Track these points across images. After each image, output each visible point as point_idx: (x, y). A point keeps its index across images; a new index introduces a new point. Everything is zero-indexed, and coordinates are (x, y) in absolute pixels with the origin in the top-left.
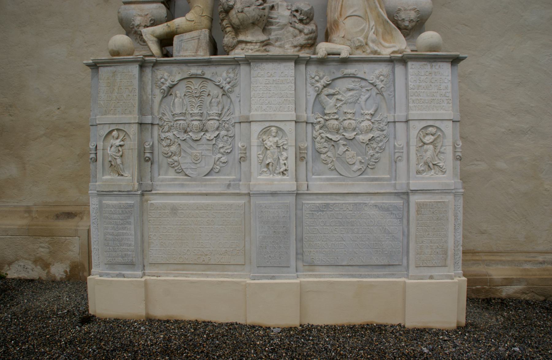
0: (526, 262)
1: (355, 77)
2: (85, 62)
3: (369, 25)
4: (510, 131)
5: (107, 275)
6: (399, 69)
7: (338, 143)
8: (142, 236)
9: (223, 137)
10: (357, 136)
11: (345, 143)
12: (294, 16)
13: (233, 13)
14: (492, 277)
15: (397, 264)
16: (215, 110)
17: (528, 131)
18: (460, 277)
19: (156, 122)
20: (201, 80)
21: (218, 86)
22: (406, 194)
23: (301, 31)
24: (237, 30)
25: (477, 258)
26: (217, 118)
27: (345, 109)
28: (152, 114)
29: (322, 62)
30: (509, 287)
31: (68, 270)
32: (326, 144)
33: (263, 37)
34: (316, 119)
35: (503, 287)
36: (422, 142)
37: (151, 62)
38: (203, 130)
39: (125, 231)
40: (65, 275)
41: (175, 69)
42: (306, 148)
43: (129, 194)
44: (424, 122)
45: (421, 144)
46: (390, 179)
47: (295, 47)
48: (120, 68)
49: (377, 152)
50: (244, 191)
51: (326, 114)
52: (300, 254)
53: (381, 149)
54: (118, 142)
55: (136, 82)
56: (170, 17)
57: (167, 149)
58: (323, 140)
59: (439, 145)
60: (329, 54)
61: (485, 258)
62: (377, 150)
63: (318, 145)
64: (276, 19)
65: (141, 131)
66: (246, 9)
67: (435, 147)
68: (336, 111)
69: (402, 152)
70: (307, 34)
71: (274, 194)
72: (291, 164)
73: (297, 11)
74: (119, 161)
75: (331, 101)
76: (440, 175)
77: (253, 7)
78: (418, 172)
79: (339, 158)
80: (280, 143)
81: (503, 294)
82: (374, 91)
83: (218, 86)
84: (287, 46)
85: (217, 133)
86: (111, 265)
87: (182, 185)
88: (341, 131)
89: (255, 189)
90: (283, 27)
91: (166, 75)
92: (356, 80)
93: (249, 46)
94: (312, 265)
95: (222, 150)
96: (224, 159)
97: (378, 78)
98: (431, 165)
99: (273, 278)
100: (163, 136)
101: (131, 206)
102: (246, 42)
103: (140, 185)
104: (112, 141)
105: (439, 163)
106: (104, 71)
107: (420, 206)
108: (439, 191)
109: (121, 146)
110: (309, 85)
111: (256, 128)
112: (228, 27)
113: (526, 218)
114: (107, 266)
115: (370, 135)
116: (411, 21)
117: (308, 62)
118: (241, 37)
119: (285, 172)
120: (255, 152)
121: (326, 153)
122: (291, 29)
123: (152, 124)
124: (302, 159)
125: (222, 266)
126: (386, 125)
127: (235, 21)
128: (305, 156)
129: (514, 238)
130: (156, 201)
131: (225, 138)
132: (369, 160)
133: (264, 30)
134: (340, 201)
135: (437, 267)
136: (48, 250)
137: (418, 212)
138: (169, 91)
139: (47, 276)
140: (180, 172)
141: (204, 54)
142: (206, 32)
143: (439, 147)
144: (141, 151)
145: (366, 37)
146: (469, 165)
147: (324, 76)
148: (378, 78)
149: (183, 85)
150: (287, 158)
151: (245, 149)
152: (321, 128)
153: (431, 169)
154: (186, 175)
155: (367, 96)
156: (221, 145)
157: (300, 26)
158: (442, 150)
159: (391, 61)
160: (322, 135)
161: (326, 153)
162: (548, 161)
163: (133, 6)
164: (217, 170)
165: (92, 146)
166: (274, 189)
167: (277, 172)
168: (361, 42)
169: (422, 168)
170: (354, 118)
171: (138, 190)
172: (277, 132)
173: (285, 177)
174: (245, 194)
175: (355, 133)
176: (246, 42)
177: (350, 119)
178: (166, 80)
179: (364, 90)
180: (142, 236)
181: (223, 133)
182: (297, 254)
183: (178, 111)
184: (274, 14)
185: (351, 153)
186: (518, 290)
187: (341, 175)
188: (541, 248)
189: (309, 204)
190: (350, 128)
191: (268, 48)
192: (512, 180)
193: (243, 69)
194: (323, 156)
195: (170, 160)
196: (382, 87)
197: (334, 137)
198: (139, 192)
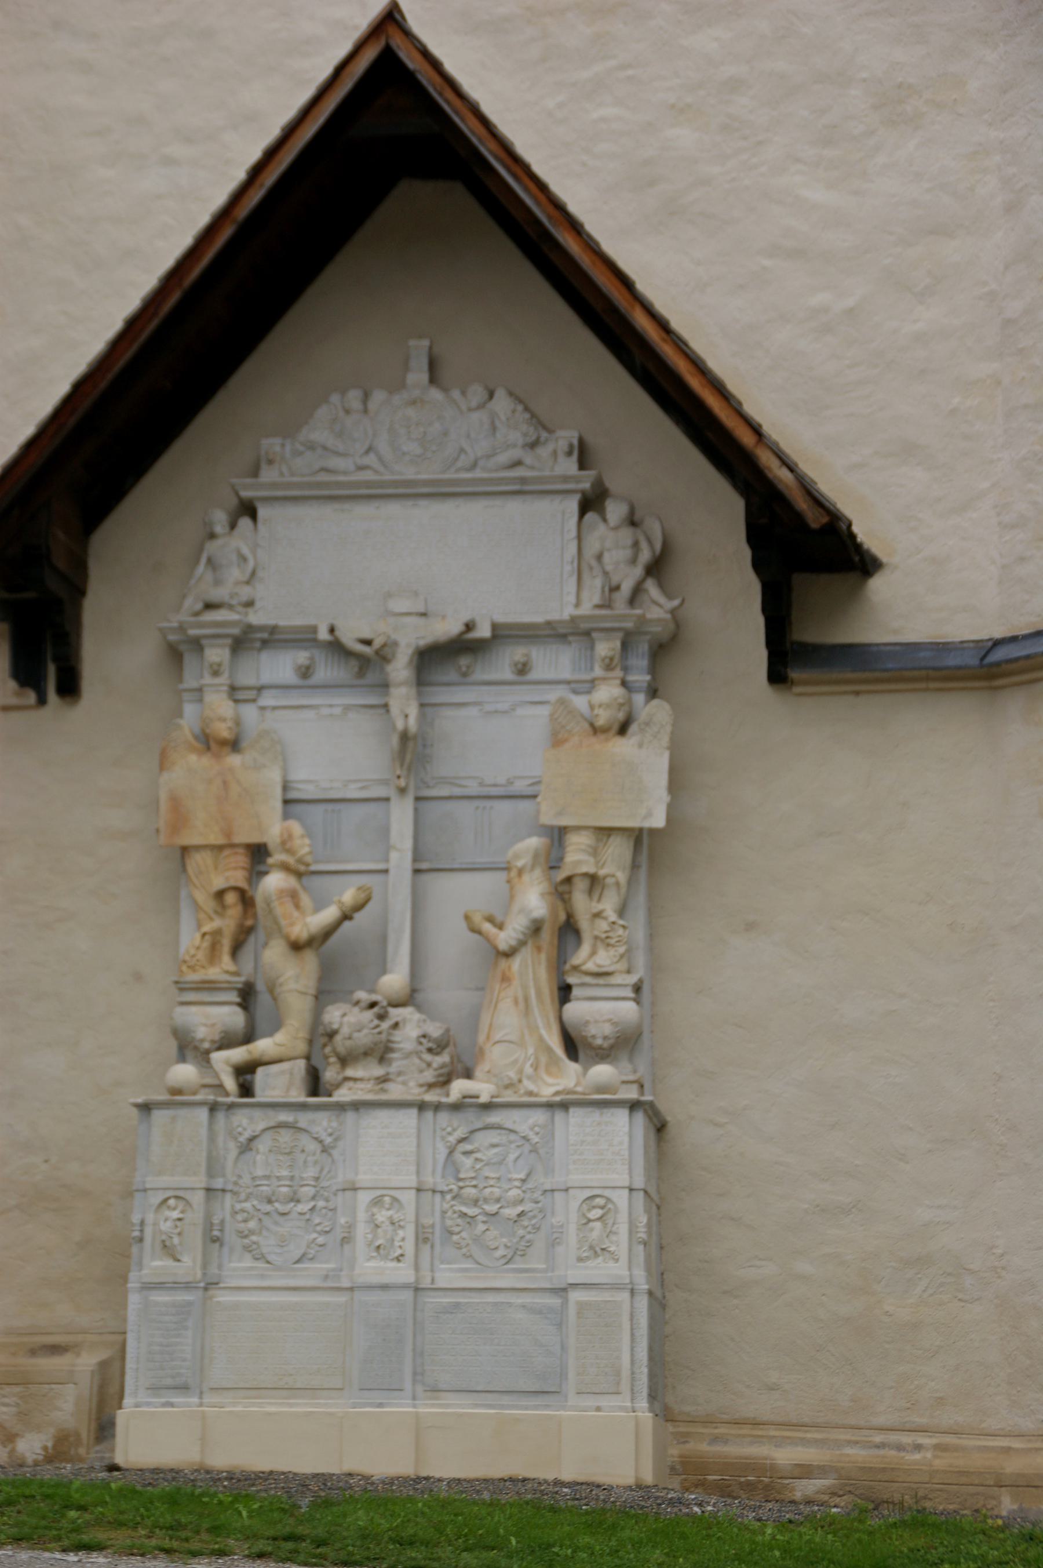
0: (849, 1443)
1: (499, 1127)
2: (132, 1100)
3: (526, 1053)
4: (818, 1208)
5: (148, 1404)
6: (559, 1116)
7: (475, 1219)
8: (202, 1348)
9: (320, 1210)
10: (502, 1210)
11: (485, 1219)
12: (421, 1043)
13: (338, 1038)
14: (774, 1462)
15: (553, 1390)
16: (311, 1172)
17: (853, 1208)
18: (643, 1412)
19: (230, 1187)
20: (292, 1131)
21: (316, 1139)
22: (561, 1291)
23: (429, 1065)
24: (344, 1061)
25: (760, 1433)
26: (312, 1183)
27: (487, 1172)
28: (224, 1176)
29: (456, 1107)
30: (807, 1480)
31: (50, 1444)
32: (459, 1221)
33: (379, 1071)
34: (448, 1185)
35: (794, 1480)
36: (586, 1218)
37: (223, 1104)
38: (295, 1199)
39: (178, 1340)
40: (43, 1453)
41: (257, 1113)
42: (433, 1226)
43: (188, 1286)
44: (589, 1190)
45: (584, 1221)
46: (545, 1271)
47: (421, 1086)
48: (183, 1112)
49: (529, 1233)
50: (346, 1283)
51: (461, 1180)
52: (418, 1375)
53: (534, 1229)
54: (175, 1214)
55: (204, 1132)
56: (248, 1037)
57: (242, 1225)
58: (456, 1215)
59: (610, 1222)
60: (464, 1097)
61: (772, 1433)
62: (529, 1229)
63: (449, 1223)
64: (398, 1042)
65: (208, 1200)
66: (356, 1035)
67: (605, 1225)
68: (473, 1175)
69: (562, 1232)
70: (436, 1070)
71: (385, 1287)
72: (409, 1247)
73: (424, 1036)
74: (176, 1240)
75: (468, 1162)
76: (611, 1264)
77: (365, 1031)
78: (580, 1259)
79: (477, 1240)
80: (396, 1217)
81: (795, 1493)
82: (527, 1148)
83: (316, 1139)
84: (412, 1084)
85: (312, 1204)
86: (155, 1389)
87: (262, 1277)
88: (480, 1203)
89: (361, 1280)
90: (408, 1055)
91: (245, 1122)
92: (503, 1132)
93: (360, 1085)
94: (435, 1390)
95: (319, 1228)
96: (321, 1240)
97: (531, 1129)
98: (598, 1249)
99: (381, 1405)
100: (238, 1206)
101: (190, 1304)
102: (355, 1080)
103: (204, 1274)
104: (167, 1213)
105: (609, 1247)
106: (159, 1116)
107: (582, 1306)
108: (608, 1286)
109: (180, 1219)
110: (438, 1139)
111: (364, 1198)
112: (332, 1056)
113: (851, 1364)
114: (149, 1391)
115: (520, 1209)
116: (605, 1038)
117: (437, 1107)
118: (350, 1072)
119: (401, 1258)
120: (362, 1230)
121: (459, 1233)
122: (417, 1061)
123: (224, 1191)
124: (426, 1240)
125: (312, 1391)
126: (542, 1195)
127: (341, 1050)
128: (430, 1236)
129: (831, 1400)
130: (223, 1298)
131: (324, 1211)
132: (518, 1243)
133: (382, 1060)
134: (476, 1299)
135: (606, 1395)
136: (14, 1409)
137: (579, 1314)
138: (248, 1144)
139: (10, 1457)
140: (261, 1257)
141: (298, 1095)
142: (301, 1064)
143: (610, 1225)
144: (209, 1226)
145: (521, 1071)
146: (744, 1268)
147: (459, 1127)
148: (531, 1129)
149: (267, 1138)
150: (403, 1239)
151: (350, 1227)
152: (454, 1198)
153: (599, 1256)
154: (268, 1262)
155: (516, 1155)
156: (317, 1221)
157: (428, 1057)
158: (614, 1229)
159: (550, 1106)
160: (455, 1208)
161: (459, 1233)
162: (890, 1262)
163: (194, 1009)
164: (311, 1256)
165: (136, 1219)
166: (385, 1280)
167: (390, 1258)
168: (510, 1078)
169: (585, 1254)
170: (498, 1185)
171: (199, 1282)
172: (391, 1204)
173: (400, 1265)
174: (347, 1289)
175: (498, 1206)
176: (355, 1080)
177: (492, 1186)
178: (245, 1129)
179: (513, 1146)
180: (202, 1348)
181: (321, 1203)
182: (415, 1374)
183: (259, 1172)
184: (397, 1036)
185: (493, 1233)
186: (823, 1488)
187: (479, 1264)
188: (881, 1420)
189: (432, 1302)
190: (492, 1199)
191: (386, 1086)
192: (824, 1295)
193: (350, 1116)
194: (455, 1238)
195: (246, 1241)
196: (537, 1143)
197: (471, 1211)
198: (202, 1285)
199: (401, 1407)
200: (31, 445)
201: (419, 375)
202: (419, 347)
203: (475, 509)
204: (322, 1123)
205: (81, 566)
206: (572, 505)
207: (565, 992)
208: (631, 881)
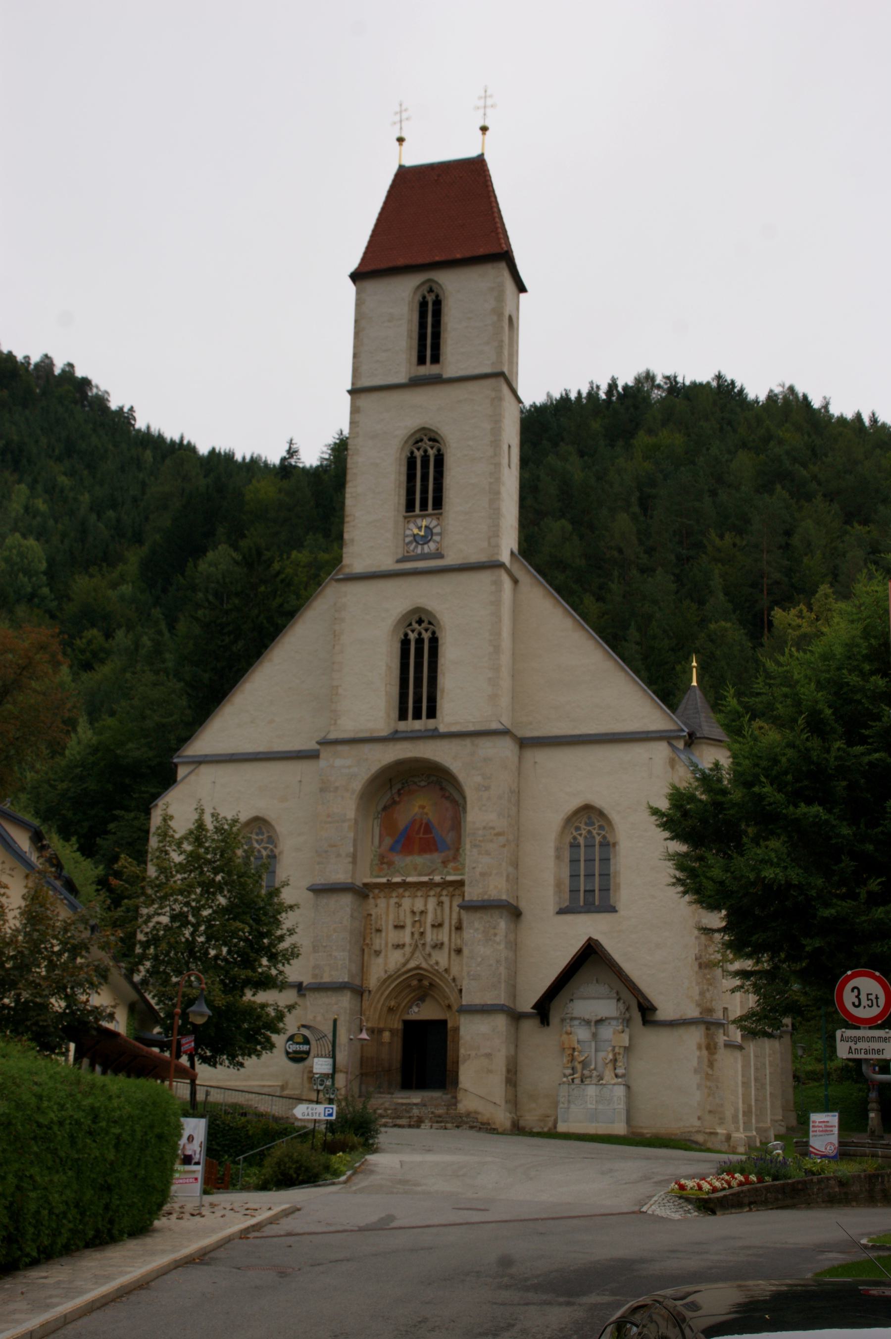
141: (580, 1083)
200: (557, 978)
201: (595, 982)
204: (583, 1087)
205: (549, 1008)
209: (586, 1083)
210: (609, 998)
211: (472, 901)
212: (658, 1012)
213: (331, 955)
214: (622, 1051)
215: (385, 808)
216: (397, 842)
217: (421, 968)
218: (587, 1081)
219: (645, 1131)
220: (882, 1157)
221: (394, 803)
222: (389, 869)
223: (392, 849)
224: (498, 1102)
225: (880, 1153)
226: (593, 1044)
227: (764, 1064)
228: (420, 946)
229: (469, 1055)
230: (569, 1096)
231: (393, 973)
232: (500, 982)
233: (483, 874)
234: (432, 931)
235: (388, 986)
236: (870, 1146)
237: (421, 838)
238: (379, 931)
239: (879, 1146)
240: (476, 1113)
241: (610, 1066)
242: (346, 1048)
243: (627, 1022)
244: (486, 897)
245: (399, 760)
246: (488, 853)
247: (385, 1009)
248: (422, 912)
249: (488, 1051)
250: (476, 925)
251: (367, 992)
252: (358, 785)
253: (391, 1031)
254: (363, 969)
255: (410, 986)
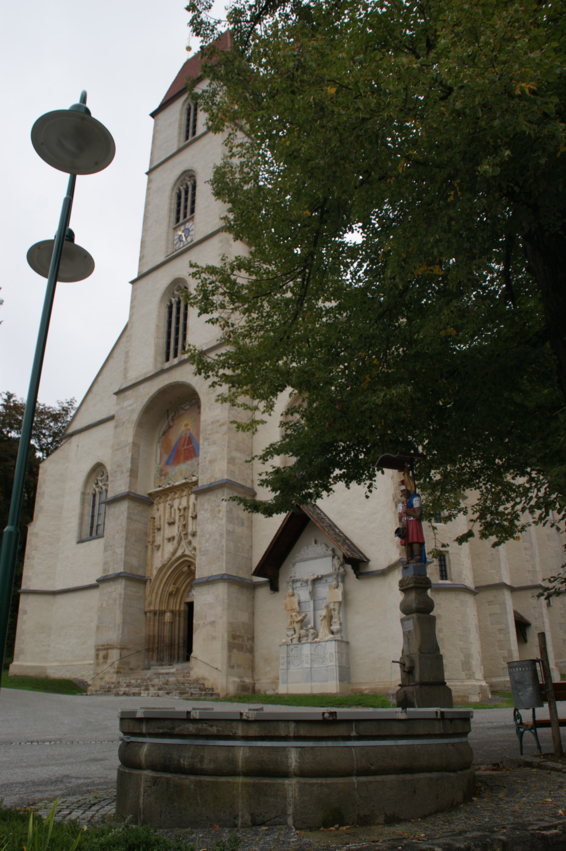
22: (327, 667)
52: (311, 679)
141: (297, 643)
144: (287, 661)
199: (309, 684)
201: (313, 543)
202: (313, 539)
203: (320, 560)
204: (300, 646)
206: (331, 558)
207: (331, 625)
208: (339, 609)
209: (302, 642)
210: (325, 556)
211: (203, 486)
212: (370, 563)
213: (114, 552)
214: (337, 606)
215: (164, 433)
216: (170, 457)
217: (186, 556)
218: (304, 640)
219: (363, 687)
220: (302, 774)
221: (170, 427)
222: (165, 478)
223: (167, 463)
224: (220, 668)
225: (293, 760)
226: (311, 603)
227: (541, 614)
228: (182, 536)
229: (199, 624)
230: (287, 656)
231: (166, 562)
232: (222, 554)
233: (211, 462)
234: (193, 522)
235: (166, 573)
236: (253, 731)
237: (185, 450)
238: (159, 529)
239: (292, 730)
240: (204, 679)
241: (325, 623)
242: (121, 628)
243: (343, 577)
244: (213, 480)
245: (160, 389)
246: (214, 443)
247: (166, 594)
248: (185, 509)
249: (212, 619)
250: (206, 506)
251: (149, 581)
252: (135, 417)
253: (172, 612)
254: (145, 563)
255: (183, 573)
